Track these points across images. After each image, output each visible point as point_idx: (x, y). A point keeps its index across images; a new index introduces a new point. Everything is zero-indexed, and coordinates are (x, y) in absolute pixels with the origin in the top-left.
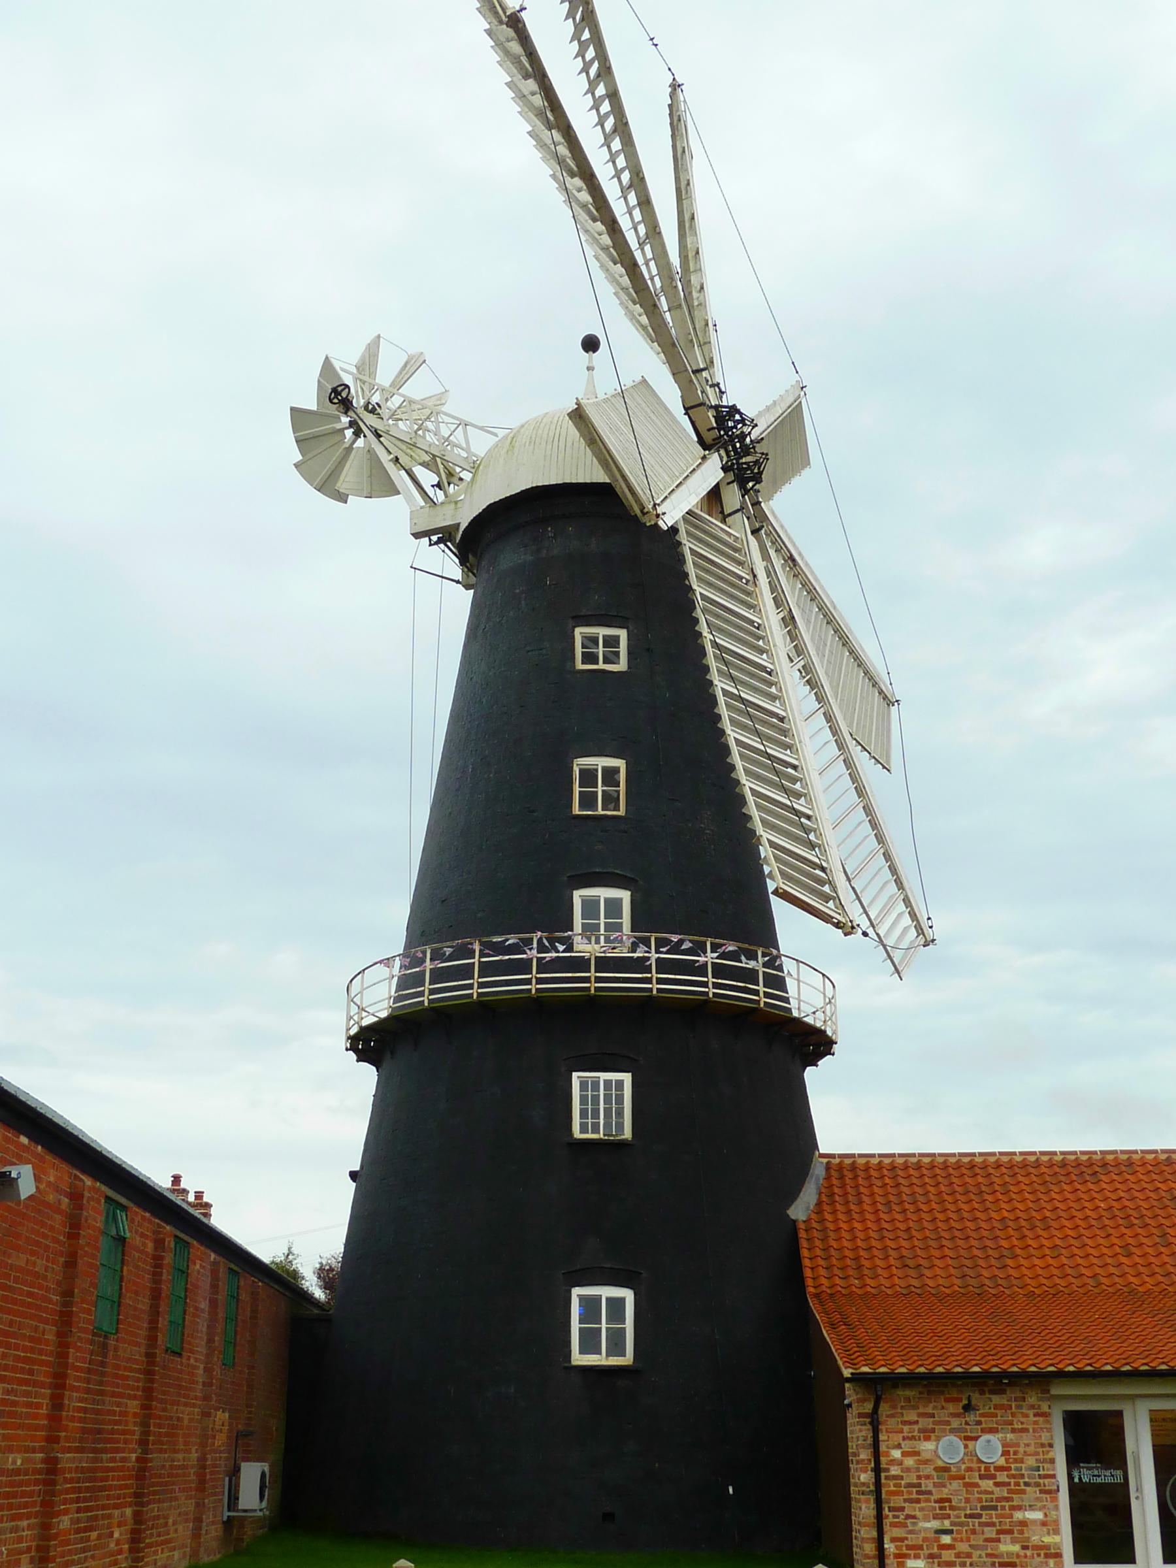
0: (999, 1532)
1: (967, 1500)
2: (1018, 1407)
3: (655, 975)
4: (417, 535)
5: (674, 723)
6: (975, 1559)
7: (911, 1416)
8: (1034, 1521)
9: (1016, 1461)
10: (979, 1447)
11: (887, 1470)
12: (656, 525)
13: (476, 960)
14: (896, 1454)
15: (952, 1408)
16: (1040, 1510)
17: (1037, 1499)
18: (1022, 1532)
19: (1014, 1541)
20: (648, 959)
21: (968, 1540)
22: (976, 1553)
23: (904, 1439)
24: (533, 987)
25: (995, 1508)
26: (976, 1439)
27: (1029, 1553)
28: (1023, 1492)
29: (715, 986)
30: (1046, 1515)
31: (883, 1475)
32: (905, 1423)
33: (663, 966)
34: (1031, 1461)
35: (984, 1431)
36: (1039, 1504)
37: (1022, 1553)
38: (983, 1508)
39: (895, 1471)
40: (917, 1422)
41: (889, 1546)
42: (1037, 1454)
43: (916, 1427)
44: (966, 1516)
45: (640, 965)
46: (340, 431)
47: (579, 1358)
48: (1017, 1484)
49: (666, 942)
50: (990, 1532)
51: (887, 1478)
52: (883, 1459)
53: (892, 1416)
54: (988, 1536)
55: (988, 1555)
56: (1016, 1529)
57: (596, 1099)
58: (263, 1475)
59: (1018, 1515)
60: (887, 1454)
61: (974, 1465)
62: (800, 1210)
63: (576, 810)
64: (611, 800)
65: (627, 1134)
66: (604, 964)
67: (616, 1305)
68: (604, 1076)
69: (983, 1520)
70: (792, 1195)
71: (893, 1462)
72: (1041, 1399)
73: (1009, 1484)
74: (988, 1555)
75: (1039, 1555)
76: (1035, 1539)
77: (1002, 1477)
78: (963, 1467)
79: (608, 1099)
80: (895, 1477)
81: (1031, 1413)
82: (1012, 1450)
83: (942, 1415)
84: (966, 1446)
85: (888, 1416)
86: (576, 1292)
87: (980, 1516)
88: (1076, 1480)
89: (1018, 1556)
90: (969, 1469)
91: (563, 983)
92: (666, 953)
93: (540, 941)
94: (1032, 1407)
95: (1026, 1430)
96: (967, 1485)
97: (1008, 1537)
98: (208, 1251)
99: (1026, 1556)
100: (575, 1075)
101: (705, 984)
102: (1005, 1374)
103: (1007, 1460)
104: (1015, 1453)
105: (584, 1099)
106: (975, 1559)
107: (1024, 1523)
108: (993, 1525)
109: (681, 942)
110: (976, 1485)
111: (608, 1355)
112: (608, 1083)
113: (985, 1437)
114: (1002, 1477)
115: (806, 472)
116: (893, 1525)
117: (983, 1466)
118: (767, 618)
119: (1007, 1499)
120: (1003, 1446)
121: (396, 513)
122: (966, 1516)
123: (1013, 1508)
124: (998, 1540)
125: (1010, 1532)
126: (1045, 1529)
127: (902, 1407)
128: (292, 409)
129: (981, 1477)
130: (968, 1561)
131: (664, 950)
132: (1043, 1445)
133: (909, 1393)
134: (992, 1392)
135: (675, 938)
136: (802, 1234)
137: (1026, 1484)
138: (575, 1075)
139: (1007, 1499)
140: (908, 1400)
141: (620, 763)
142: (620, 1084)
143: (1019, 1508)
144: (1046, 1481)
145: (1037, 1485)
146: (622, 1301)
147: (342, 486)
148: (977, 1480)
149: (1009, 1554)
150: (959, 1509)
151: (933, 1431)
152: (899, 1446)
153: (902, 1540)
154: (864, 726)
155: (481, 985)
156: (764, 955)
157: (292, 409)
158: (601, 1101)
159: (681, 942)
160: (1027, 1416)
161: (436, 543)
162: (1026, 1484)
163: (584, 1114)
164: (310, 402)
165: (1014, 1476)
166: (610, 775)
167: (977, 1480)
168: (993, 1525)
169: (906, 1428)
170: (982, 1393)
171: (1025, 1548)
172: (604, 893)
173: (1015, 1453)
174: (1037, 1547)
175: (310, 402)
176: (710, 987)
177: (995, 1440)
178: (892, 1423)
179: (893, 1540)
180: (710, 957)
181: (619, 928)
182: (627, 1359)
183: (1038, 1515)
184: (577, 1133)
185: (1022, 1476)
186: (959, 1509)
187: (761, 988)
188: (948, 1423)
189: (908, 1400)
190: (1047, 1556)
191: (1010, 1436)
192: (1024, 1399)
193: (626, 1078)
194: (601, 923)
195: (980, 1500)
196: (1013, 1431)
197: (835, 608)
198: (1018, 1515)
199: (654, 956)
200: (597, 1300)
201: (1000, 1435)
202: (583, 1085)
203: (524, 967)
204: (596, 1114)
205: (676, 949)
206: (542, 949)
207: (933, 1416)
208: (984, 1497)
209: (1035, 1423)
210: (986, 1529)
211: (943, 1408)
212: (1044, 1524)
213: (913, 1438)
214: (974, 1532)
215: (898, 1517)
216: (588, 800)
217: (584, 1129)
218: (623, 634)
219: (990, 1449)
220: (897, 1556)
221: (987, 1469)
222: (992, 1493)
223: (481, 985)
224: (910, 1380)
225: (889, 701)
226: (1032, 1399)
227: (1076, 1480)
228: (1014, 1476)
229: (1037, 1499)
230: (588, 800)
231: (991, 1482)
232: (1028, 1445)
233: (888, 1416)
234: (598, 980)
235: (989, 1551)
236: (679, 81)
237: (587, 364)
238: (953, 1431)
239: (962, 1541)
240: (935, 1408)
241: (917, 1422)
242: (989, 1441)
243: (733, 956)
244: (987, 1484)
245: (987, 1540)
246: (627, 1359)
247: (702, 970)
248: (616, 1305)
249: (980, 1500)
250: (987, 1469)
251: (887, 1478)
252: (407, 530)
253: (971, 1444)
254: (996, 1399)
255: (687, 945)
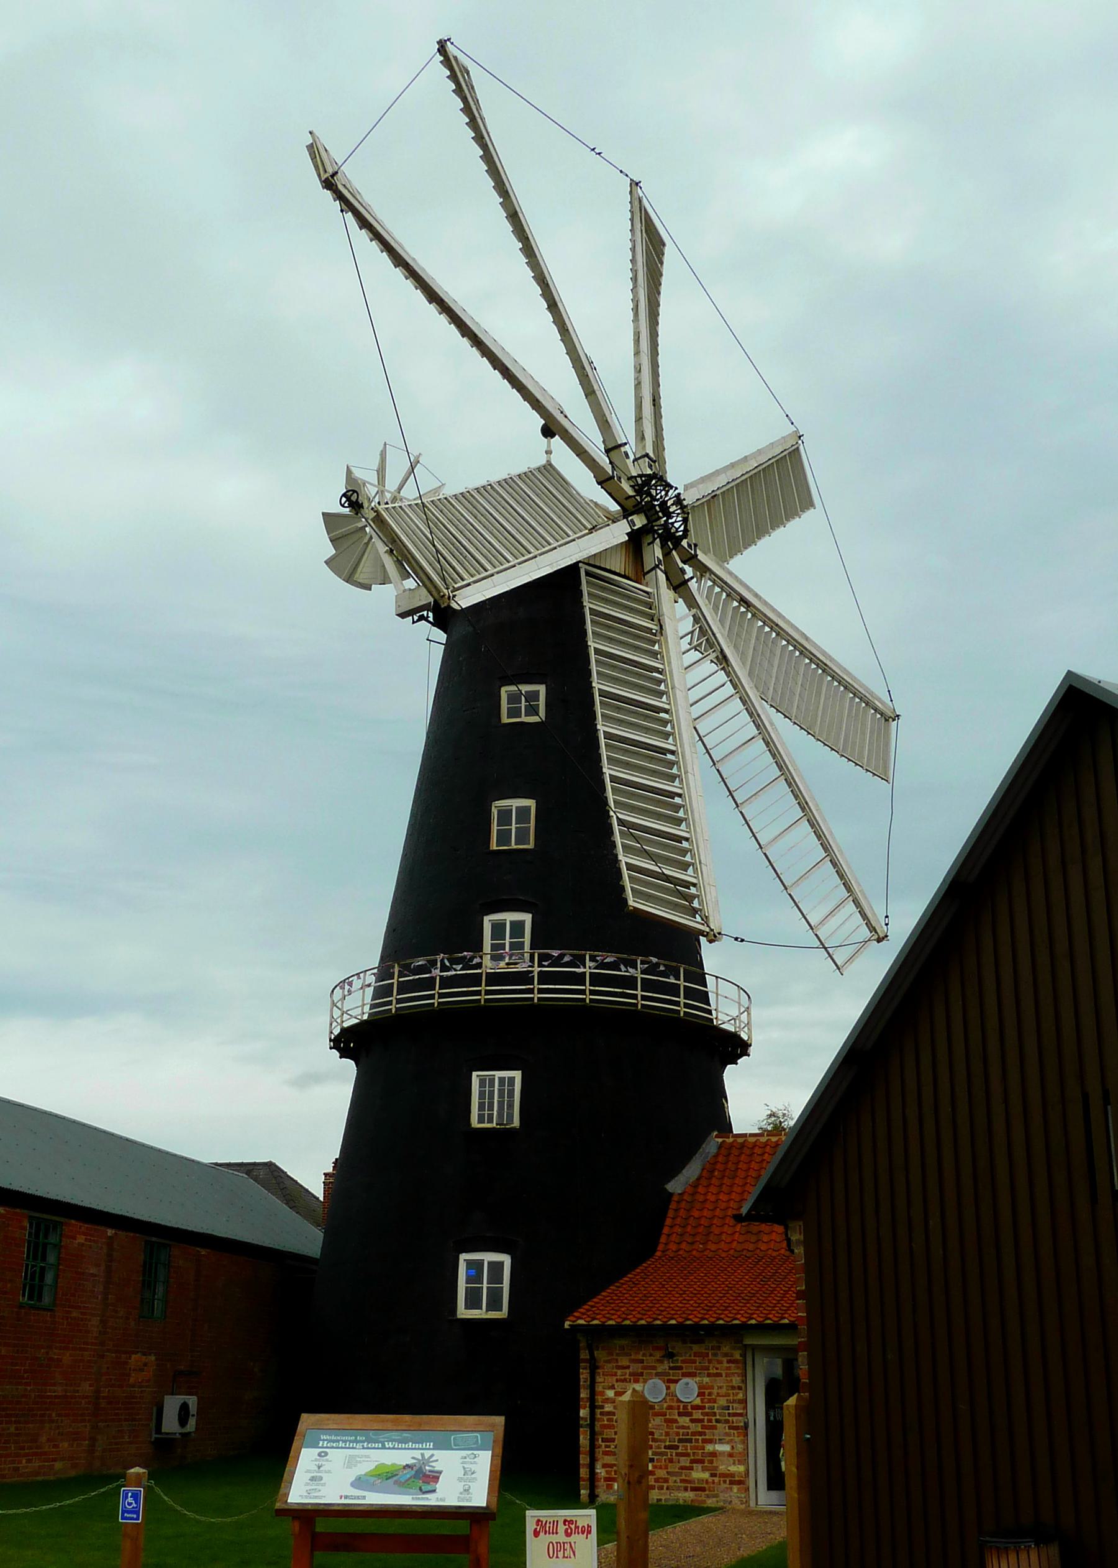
0: (692, 1462)
1: (667, 1434)
2: (715, 1355)
3: (537, 987)
4: (403, 615)
5: (564, 766)
6: (671, 1484)
7: (624, 1362)
8: (722, 1453)
9: (709, 1401)
10: (678, 1389)
11: (602, 1407)
12: (449, 606)
13: (395, 981)
14: (610, 1394)
15: (658, 1354)
16: (728, 1443)
17: (727, 1434)
18: (711, 1462)
19: (704, 1470)
20: (532, 972)
21: (666, 1467)
22: (672, 1479)
23: (617, 1381)
24: (435, 1001)
25: (690, 1441)
26: (676, 1382)
27: (716, 1479)
28: (715, 1428)
29: (592, 992)
30: (733, 1448)
31: (598, 1411)
32: (618, 1367)
33: (544, 978)
34: (722, 1402)
35: (685, 1375)
36: (728, 1438)
37: (710, 1480)
38: (680, 1441)
39: (608, 1408)
40: (628, 1367)
41: (600, 1471)
42: (728, 1395)
43: (628, 1371)
44: (665, 1447)
45: (524, 978)
46: (361, 531)
47: (463, 1312)
48: (710, 1421)
49: (547, 957)
50: (685, 1462)
51: (602, 1414)
52: (599, 1398)
53: (609, 1362)
54: (683, 1464)
55: (682, 1481)
56: (706, 1459)
57: (492, 1093)
58: (184, 1407)
59: (709, 1448)
60: (603, 1394)
61: (675, 1404)
62: (675, 1186)
63: (494, 846)
64: (522, 836)
65: (516, 1123)
66: (495, 978)
67: (496, 1267)
68: (499, 1074)
69: (680, 1451)
70: (674, 1171)
71: (607, 1400)
72: (734, 1348)
73: (702, 1421)
74: (682, 1481)
75: (725, 1482)
76: (722, 1468)
77: (697, 1415)
78: (665, 1405)
79: (501, 1092)
80: (609, 1413)
81: (725, 1359)
82: (707, 1392)
83: (650, 1361)
84: (668, 1388)
85: (606, 1362)
86: (463, 1257)
87: (677, 1447)
88: (772, 1418)
89: (707, 1482)
90: (670, 1408)
91: (460, 996)
92: (548, 966)
93: (442, 961)
94: (726, 1355)
95: (720, 1375)
96: (667, 1421)
97: (700, 1466)
98: (103, 1228)
99: (713, 1482)
100: (474, 1074)
101: (583, 992)
102: (697, 1327)
103: (702, 1401)
104: (710, 1394)
105: (482, 1095)
106: (671, 1484)
107: (714, 1454)
108: (688, 1455)
109: (562, 956)
110: (676, 1421)
111: (487, 1310)
112: (502, 1080)
113: (685, 1380)
114: (697, 1415)
115: (809, 514)
116: (606, 1453)
117: (682, 1405)
118: (669, 663)
119: (701, 1434)
120: (699, 1388)
121: (385, 597)
122: (665, 1447)
123: (705, 1441)
124: (691, 1469)
125: (701, 1462)
126: (731, 1460)
127: (618, 1355)
128: (323, 514)
129: (680, 1414)
130: (665, 1485)
131: (546, 963)
132: (733, 1388)
133: (623, 1342)
134: (693, 1342)
135: (555, 953)
136: (673, 1206)
137: (717, 1421)
138: (474, 1074)
139: (701, 1434)
140: (622, 1348)
141: (531, 803)
142: (512, 1080)
143: (710, 1441)
144: (735, 1419)
145: (727, 1421)
146: (501, 1264)
147: (360, 576)
148: (676, 1417)
149: (700, 1480)
150: (661, 1441)
151: (642, 1374)
152: (613, 1387)
153: (611, 1466)
154: (854, 743)
155: (441, 996)
156: (642, 963)
157: (323, 514)
158: (495, 1096)
159: (562, 956)
160: (721, 1362)
161: (418, 620)
162: (717, 1421)
163: (481, 1107)
164: (336, 507)
165: (707, 1414)
166: (523, 812)
167: (676, 1417)
168: (688, 1455)
169: (619, 1372)
170: (684, 1342)
171: (712, 1475)
172: (509, 917)
173: (710, 1394)
174: (723, 1475)
175: (336, 507)
176: (587, 993)
177: (693, 1384)
178: (608, 1367)
179: (604, 1466)
180: (589, 968)
181: (521, 946)
182: (503, 1314)
183: (726, 1448)
184: (475, 1123)
185: (715, 1414)
186: (661, 1441)
187: (639, 993)
188: (654, 1368)
189: (622, 1348)
190: (731, 1483)
191: (706, 1380)
192: (719, 1348)
193: (517, 1075)
194: (507, 940)
195: (678, 1434)
196: (709, 1375)
197: (807, 639)
198: (709, 1448)
199: (536, 969)
200: (480, 1263)
201: (698, 1379)
202: (482, 1083)
203: (429, 984)
204: (491, 1108)
205: (556, 962)
206: (444, 968)
207: (642, 1361)
208: (681, 1431)
209: (728, 1368)
210: (682, 1458)
211: (651, 1355)
212: (731, 1455)
213: (624, 1380)
214: (671, 1461)
215: (609, 1447)
216: (504, 837)
217: (481, 1119)
218: (542, 689)
219: (687, 1390)
220: (606, 1479)
221: (685, 1407)
222: (688, 1428)
223: (540, 991)
224: (619, 1331)
225: (890, 718)
226: (726, 1349)
227: (772, 1418)
228: (707, 1414)
229: (727, 1434)
230: (504, 837)
231: (687, 1419)
232: (721, 1387)
233: (606, 1362)
234: (488, 992)
235: (683, 1477)
236: (636, 180)
237: (545, 448)
238: (657, 1375)
239: (661, 1468)
240: (644, 1355)
241: (628, 1367)
242: (687, 1384)
243: (614, 966)
244: (684, 1421)
245: (682, 1468)
246: (503, 1314)
247: (579, 979)
248: (496, 1267)
249: (678, 1434)
250: (685, 1407)
251: (602, 1414)
252: (393, 611)
253: (672, 1386)
254: (696, 1348)
255: (567, 959)
